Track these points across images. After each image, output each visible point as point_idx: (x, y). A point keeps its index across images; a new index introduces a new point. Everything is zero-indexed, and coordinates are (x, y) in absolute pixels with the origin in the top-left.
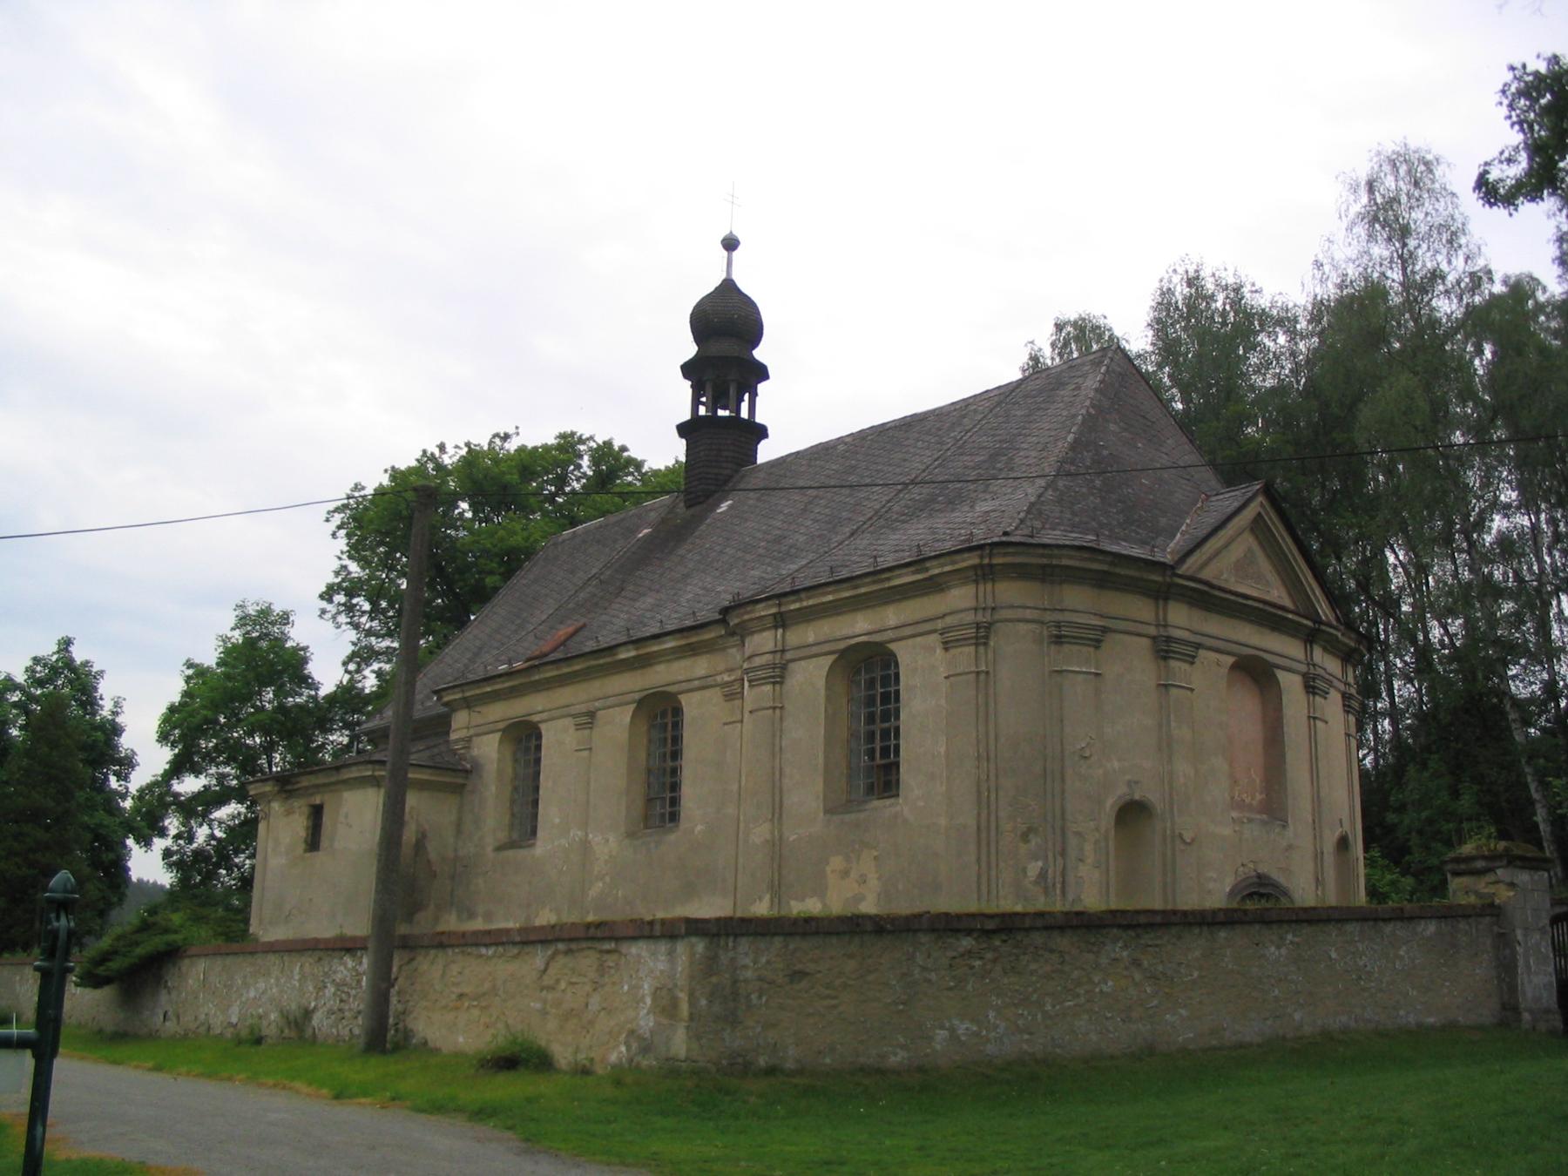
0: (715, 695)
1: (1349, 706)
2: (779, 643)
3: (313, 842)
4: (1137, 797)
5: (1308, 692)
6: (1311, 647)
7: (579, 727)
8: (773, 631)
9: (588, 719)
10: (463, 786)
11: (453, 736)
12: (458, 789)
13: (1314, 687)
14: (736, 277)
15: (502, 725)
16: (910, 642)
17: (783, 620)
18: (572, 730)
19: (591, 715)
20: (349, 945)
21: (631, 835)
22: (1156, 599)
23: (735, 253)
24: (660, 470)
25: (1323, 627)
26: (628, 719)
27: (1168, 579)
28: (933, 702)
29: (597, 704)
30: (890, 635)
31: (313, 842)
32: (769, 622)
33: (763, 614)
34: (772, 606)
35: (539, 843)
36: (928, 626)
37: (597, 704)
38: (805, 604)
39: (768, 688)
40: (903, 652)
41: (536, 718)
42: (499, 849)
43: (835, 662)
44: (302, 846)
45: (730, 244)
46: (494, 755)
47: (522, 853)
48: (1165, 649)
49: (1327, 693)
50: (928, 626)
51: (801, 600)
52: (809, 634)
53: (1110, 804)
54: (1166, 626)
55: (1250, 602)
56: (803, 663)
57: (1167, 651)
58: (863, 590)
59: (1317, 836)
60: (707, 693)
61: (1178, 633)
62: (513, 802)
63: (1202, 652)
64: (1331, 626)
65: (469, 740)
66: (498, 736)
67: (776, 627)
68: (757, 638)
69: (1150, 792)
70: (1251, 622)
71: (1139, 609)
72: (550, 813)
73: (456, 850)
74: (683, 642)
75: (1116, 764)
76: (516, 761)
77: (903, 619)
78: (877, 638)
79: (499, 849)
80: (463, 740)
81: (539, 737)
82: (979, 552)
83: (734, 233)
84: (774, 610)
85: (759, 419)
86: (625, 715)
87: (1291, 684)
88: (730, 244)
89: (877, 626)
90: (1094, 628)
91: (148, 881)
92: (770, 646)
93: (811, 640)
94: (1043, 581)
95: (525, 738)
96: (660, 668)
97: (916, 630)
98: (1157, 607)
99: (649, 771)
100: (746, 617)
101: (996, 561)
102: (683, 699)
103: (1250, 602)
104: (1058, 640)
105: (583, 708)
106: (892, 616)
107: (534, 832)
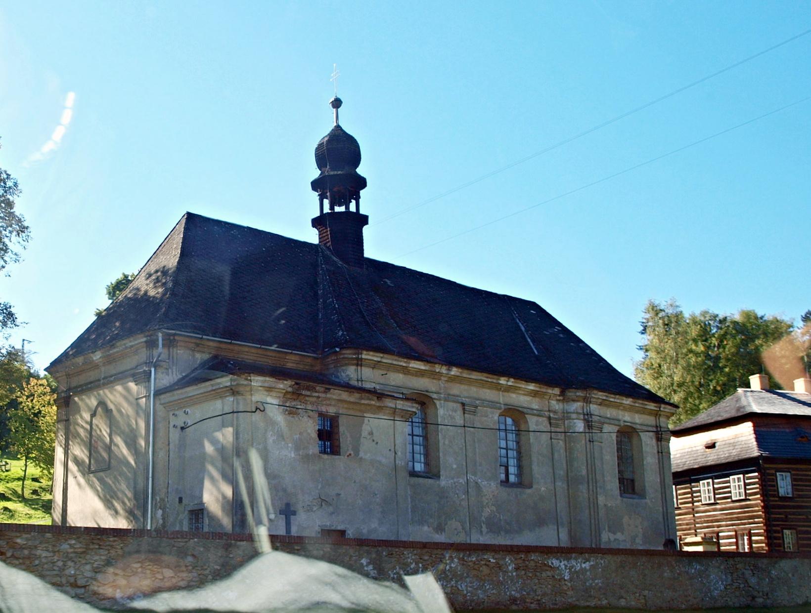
14: (340, 124)
88: (337, 103)
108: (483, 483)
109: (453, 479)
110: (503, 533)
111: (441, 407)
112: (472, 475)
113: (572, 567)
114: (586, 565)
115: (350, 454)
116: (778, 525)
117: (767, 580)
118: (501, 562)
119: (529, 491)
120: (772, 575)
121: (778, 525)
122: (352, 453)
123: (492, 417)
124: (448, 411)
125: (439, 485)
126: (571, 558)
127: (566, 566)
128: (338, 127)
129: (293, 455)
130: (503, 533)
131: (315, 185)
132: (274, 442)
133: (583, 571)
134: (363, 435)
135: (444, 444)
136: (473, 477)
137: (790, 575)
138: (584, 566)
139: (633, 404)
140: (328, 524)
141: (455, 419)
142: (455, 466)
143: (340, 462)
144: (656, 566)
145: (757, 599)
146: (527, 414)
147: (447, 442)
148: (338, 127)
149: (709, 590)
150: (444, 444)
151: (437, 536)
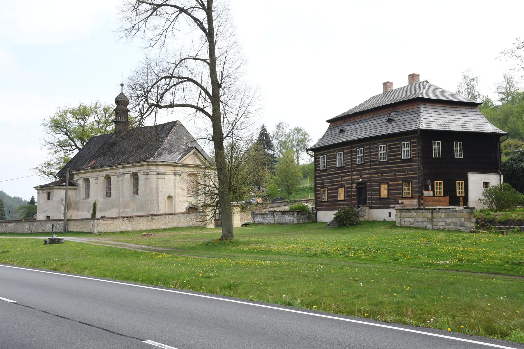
0: (116, 177)
3: (49, 198)
7: (96, 180)
9: (97, 179)
11: (74, 179)
12: (76, 189)
15: (83, 178)
19: (97, 178)
21: (104, 198)
24: (12, 197)
26: (103, 179)
30: (137, 172)
31: (49, 198)
35: (90, 198)
37: (98, 176)
41: (89, 178)
42: (83, 199)
44: (46, 199)
46: (82, 183)
47: (87, 200)
50: (142, 171)
52: (127, 170)
53: (166, 196)
60: (115, 176)
62: (85, 191)
65: (77, 180)
66: (130, 174)
69: (172, 194)
72: (91, 193)
76: (85, 184)
78: (136, 172)
79: (83, 199)
81: (111, 178)
86: (103, 179)
90: (164, 172)
93: (128, 171)
95: (87, 180)
97: (93, 177)
102: (111, 176)
104: (158, 174)
105: (96, 177)
106: (138, 169)
107: (89, 196)
116: (319, 187)
119: (110, 199)
121: (319, 187)
128: (122, 94)
148: (122, 94)
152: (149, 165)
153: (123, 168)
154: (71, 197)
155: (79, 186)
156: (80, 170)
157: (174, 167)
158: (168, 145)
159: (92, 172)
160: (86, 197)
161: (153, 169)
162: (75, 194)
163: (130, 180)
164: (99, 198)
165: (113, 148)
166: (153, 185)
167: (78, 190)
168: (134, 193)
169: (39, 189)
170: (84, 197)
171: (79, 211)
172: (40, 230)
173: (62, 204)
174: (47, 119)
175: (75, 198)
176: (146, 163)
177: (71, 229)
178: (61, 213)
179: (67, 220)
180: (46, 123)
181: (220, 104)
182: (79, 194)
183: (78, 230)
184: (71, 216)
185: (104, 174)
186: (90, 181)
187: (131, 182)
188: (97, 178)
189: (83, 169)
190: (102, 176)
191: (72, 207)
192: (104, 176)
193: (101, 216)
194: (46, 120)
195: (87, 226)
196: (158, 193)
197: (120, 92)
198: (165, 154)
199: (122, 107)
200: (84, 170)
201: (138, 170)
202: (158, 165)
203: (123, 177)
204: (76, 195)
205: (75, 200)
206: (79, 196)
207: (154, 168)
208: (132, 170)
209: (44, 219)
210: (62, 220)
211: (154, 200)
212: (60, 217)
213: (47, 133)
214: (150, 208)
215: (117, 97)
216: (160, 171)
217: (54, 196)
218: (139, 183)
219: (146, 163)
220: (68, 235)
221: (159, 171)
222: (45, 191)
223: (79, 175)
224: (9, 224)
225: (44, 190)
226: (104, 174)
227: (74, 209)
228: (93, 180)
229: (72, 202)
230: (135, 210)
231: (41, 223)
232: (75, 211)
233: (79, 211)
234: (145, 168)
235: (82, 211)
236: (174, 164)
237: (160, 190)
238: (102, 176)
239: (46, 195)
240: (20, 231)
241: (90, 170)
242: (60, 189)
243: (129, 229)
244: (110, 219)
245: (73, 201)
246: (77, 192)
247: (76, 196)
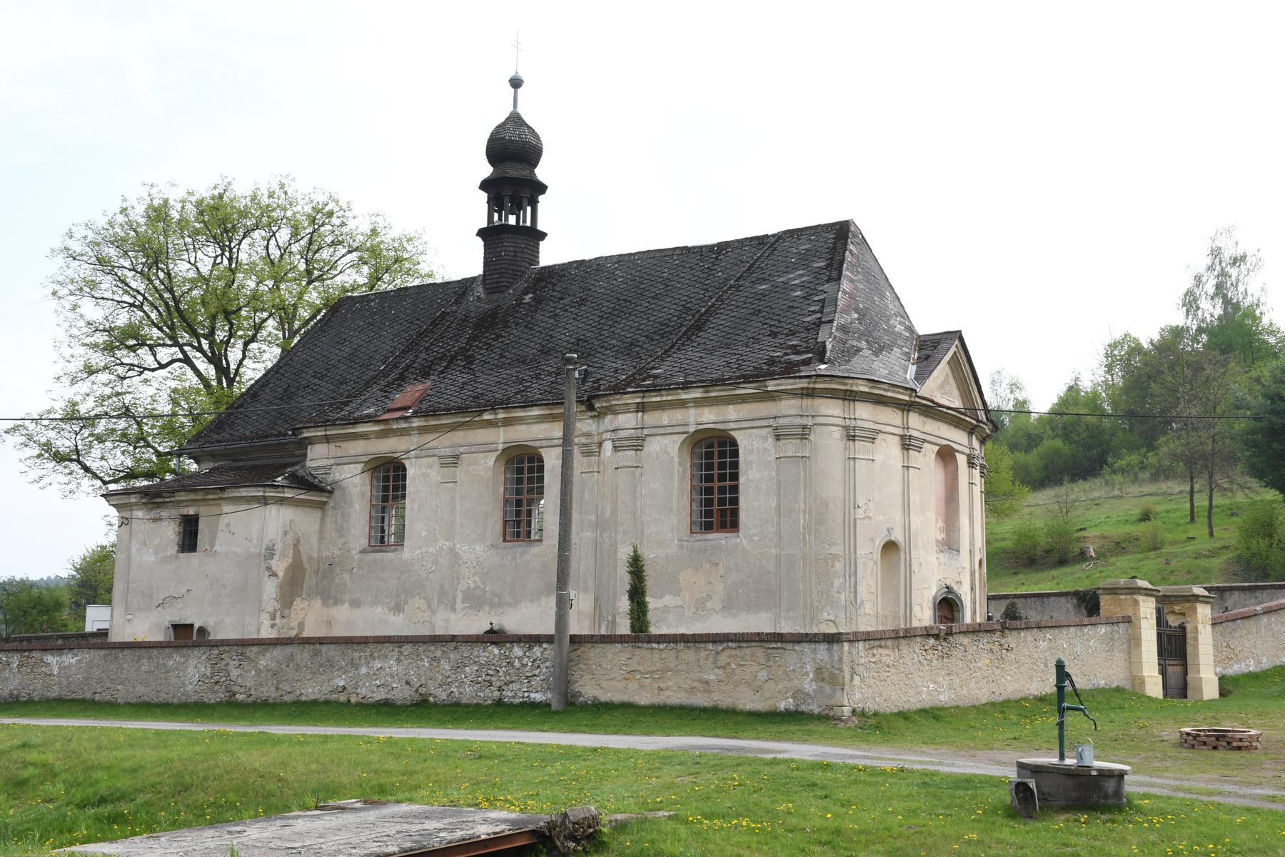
1: (983, 473)
2: (639, 423)
4: (893, 539)
5: (969, 467)
6: (908, 415)
8: (635, 414)
10: (325, 503)
11: (309, 464)
12: (322, 506)
13: (973, 463)
14: (519, 110)
16: (748, 432)
17: (643, 407)
18: (437, 467)
19: (457, 457)
20: (796, 639)
22: (903, 410)
23: (519, 90)
25: (981, 424)
26: (491, 462)
27: (913, 399)
28: (766, 474)
29: (462, 450)
30: (732, 426)
32: (633, 408)
33: (628, 402)
34: (638, 397)
36: (765, 423)
37: (462, 450)
38: (664, 398)
39: (632, 453)
40: (742, 439)
43: (686, 438)
45: (516, 83)
48: (907, 443)
49: (921, 448)
50: (765, 423)
51: (662, 396)
52: (665, 417)
53: (879, 543)
54: (908, 428)
55: (950, 411)
56: (659, 437)
57: (909, 445)
58: (713, 394)
59: (972, 561)
61: (915, 434)
63: (926, 445)
64: (984, 423)
67: (637, 412)
68: (621, 418)
69: (898, 536)
70: (946, 422)
71: (891, 417)
73: (319, 551)
74: (548, 412)
75: (882, 518)
77: (741, 416)
80: (324, 467)
82: (808, 380)
83: (519, 74)
84: (638, 400)
85: (540, 227)
86: (491, 460)
87: (962, 460)
88: (516, 83)
89: (721, 419)
91: (49, 578)
92: (633, 424)
93: (665, 422)
94: (844, 399)
96: (523, 428)
97: (752, 424)
98: (903, 414)
99: (506, 501)
100: (614, 403)
101: (817, 386)
103: (950, 411)
105: (448, 451)
106: (732, 412)
108: (464, 548)
109: (420, 548)
110: (486, 608)
111: (412, 466)
112: (446, 541)
113: (62, 662)
114: (73, 661)
115: (206, 550)
117: (253, 672)
118: (11, 660)
120: (259, 667)
122: (208, 548)
123: (485, 463)
124: (420, 469)
125: (401, 558)
126: (62, 654)
127: (58, 661)
128: (515, 120)
129: (153, 559)
130: (486, 608)
131: (485, 185)
132: (137, 550)
133: (70, 665)
134: (220, 528)
135: (412, 509)
136: (447, 543)
137: (284, 666)
138: (72, 660)
139: (704, 395)
140: (177, 619)
141: (429, 476)
142: (424, 534)
143: (193, 558)
144: (136, 658)
145: (237, 696)
146: (542, 447)
147: (416, 507)
148: (515, 120)
149: (184, 684)
150: (412, 509)
151: (393, 618)
152: (810, 393)
153: (641, 408)
154: (302, 542)
155: (337, 493)
156: (356, 422)
157: (899, 413)
158: (856, 316)
159: (423, 430)
160: (373, 543)
161: (830, 412)
162: (317, 527)
163: (680, 464)
164: (463, 549)
165: (499, 336)
166: (833, 488)
167: (330, 512)
168: (692, 523)
169: (136, 504)
170: (364, 542)
171: (336, 603)
172: (311, 691)
173: (268, 569)
174: (80, 232)
175: (315, 544)
176: (803, 384)
177: (589, 689)
178: (260, 610)
179: (575, 640)
180: (76, 247)
181: (382, 287)
182: (341, 531)
183: (675, 697)
184: (301, 626)
185: (503, 437)
186: (410, 472)
187: (684, 472)
188: (457, 457)
189: (369, 419)
190: (486, 448)
191: (305, 586)
192: (501, 447)
193: (488, 627)
194: (77, 236)
195: (763, 675)
196: (851, 526)
197: (511, 109)
198: (859, 350)
199: (514, 171)
200: (379, 422)
201: (733, 417)
202: (849, 397)
203: (638, 448)
204: (321, 532)
205: (315, 555)
206: (341, 536)
207: (831, 409)
208: (692, 419)
209: (160, 637)
210: (549, 639)
211: (835, 557)
212: (258, 631)
213: (54, 294)
214: (815, 596)
215: (501, 127)
216: (859, 423)
217: (220, 534)
218: (742, 480)
219: (803, 384)
220: (933, 742)
221: (853, 423)
222: (164, 513)
223: (343, 445)
224: (50, 659)
225: (159, 505)
226: (503, 437)
227: (310, 597)
228: (765, 438)
229: (306, 565)
230: (715, 603)
231: (316, 654)
232: (317, 603)
233: (338, 602)
234: (788, 407)
235: (355, 604)
236: (907, 398)
237: (860, 513)
238: (486, 448)
239: (170, 531)
240: (141, 690)
241: (416, 423)
242: (264, 501)
243: (941, 697)
244: (889, 643)
245: (310, 558)
246: (328, 520)
247: (321, 538)
